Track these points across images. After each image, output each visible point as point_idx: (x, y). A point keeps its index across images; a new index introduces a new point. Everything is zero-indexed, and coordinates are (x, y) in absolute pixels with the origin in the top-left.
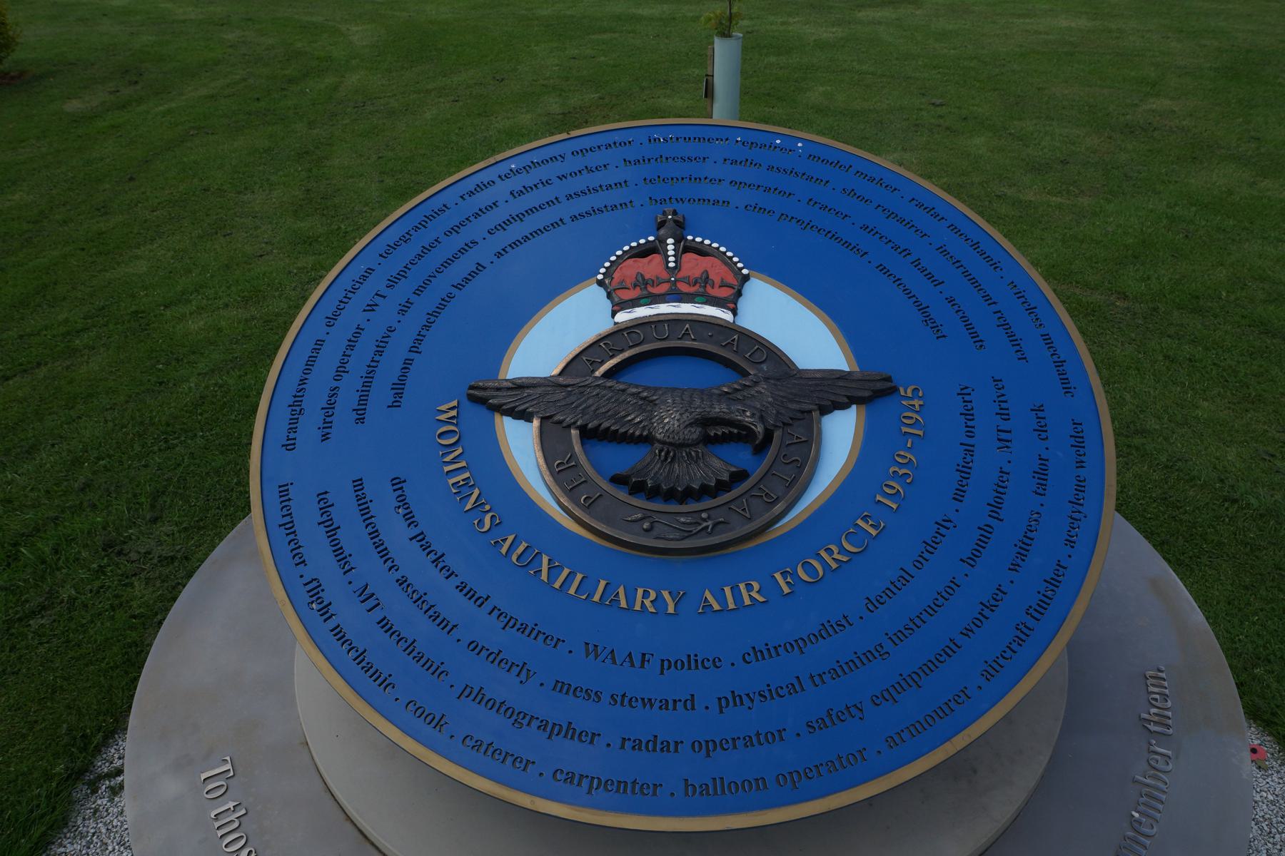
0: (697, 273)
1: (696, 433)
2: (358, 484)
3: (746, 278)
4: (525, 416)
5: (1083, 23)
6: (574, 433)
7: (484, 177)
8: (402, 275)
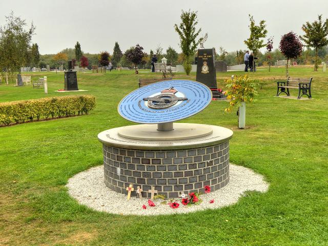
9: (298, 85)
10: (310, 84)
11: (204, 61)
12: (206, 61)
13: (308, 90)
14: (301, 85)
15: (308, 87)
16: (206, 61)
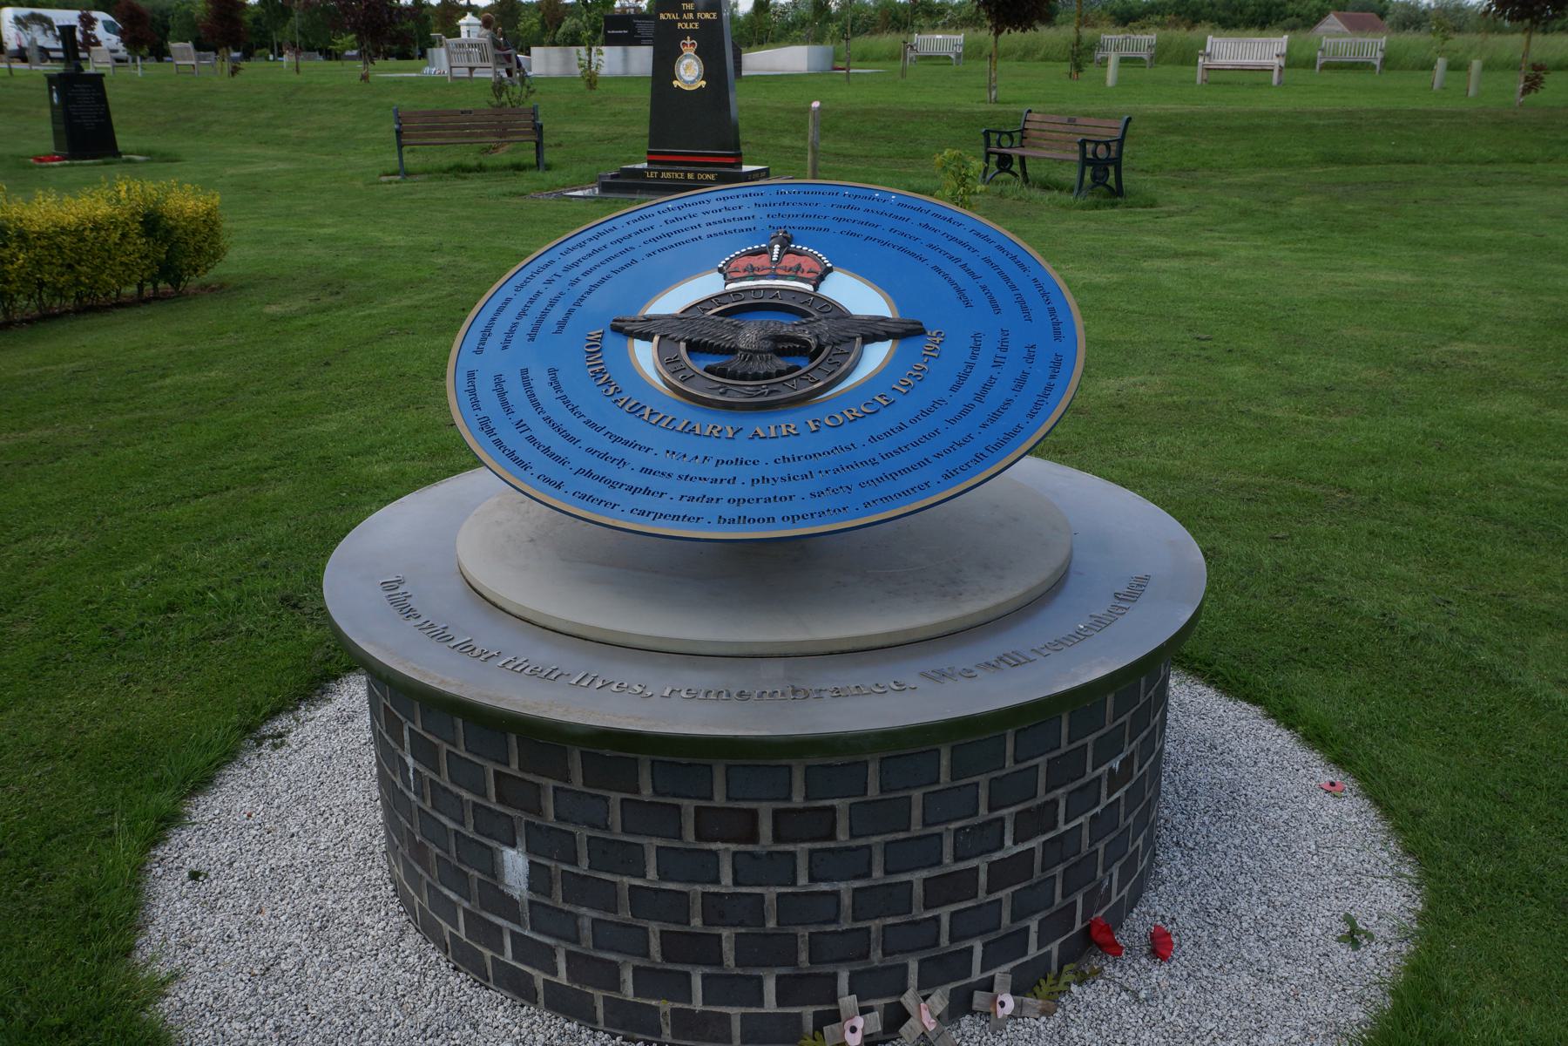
0: (793, 264)
1: (768, 345)
2: (525, 372)
3: (829, 270)
4: (647, 337)
5: (1406, 278)
6: (683, 344)
7: (647, 212)
8: (576, 264)
9: (1077, 148)
10: (1121, 142)
11: (684, 34)
12: (693, 34)
13: (1111, 169)
14: (1089, 147)
15: (1113, 154)
16: (693, 34)
